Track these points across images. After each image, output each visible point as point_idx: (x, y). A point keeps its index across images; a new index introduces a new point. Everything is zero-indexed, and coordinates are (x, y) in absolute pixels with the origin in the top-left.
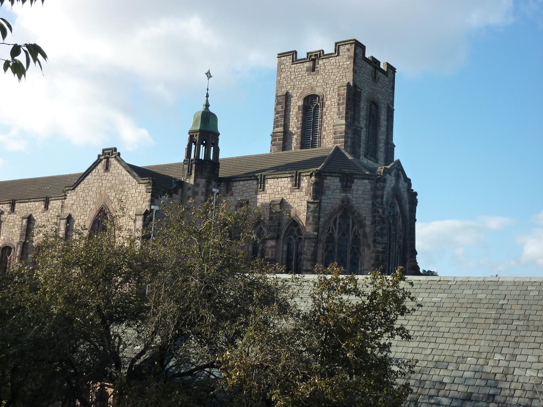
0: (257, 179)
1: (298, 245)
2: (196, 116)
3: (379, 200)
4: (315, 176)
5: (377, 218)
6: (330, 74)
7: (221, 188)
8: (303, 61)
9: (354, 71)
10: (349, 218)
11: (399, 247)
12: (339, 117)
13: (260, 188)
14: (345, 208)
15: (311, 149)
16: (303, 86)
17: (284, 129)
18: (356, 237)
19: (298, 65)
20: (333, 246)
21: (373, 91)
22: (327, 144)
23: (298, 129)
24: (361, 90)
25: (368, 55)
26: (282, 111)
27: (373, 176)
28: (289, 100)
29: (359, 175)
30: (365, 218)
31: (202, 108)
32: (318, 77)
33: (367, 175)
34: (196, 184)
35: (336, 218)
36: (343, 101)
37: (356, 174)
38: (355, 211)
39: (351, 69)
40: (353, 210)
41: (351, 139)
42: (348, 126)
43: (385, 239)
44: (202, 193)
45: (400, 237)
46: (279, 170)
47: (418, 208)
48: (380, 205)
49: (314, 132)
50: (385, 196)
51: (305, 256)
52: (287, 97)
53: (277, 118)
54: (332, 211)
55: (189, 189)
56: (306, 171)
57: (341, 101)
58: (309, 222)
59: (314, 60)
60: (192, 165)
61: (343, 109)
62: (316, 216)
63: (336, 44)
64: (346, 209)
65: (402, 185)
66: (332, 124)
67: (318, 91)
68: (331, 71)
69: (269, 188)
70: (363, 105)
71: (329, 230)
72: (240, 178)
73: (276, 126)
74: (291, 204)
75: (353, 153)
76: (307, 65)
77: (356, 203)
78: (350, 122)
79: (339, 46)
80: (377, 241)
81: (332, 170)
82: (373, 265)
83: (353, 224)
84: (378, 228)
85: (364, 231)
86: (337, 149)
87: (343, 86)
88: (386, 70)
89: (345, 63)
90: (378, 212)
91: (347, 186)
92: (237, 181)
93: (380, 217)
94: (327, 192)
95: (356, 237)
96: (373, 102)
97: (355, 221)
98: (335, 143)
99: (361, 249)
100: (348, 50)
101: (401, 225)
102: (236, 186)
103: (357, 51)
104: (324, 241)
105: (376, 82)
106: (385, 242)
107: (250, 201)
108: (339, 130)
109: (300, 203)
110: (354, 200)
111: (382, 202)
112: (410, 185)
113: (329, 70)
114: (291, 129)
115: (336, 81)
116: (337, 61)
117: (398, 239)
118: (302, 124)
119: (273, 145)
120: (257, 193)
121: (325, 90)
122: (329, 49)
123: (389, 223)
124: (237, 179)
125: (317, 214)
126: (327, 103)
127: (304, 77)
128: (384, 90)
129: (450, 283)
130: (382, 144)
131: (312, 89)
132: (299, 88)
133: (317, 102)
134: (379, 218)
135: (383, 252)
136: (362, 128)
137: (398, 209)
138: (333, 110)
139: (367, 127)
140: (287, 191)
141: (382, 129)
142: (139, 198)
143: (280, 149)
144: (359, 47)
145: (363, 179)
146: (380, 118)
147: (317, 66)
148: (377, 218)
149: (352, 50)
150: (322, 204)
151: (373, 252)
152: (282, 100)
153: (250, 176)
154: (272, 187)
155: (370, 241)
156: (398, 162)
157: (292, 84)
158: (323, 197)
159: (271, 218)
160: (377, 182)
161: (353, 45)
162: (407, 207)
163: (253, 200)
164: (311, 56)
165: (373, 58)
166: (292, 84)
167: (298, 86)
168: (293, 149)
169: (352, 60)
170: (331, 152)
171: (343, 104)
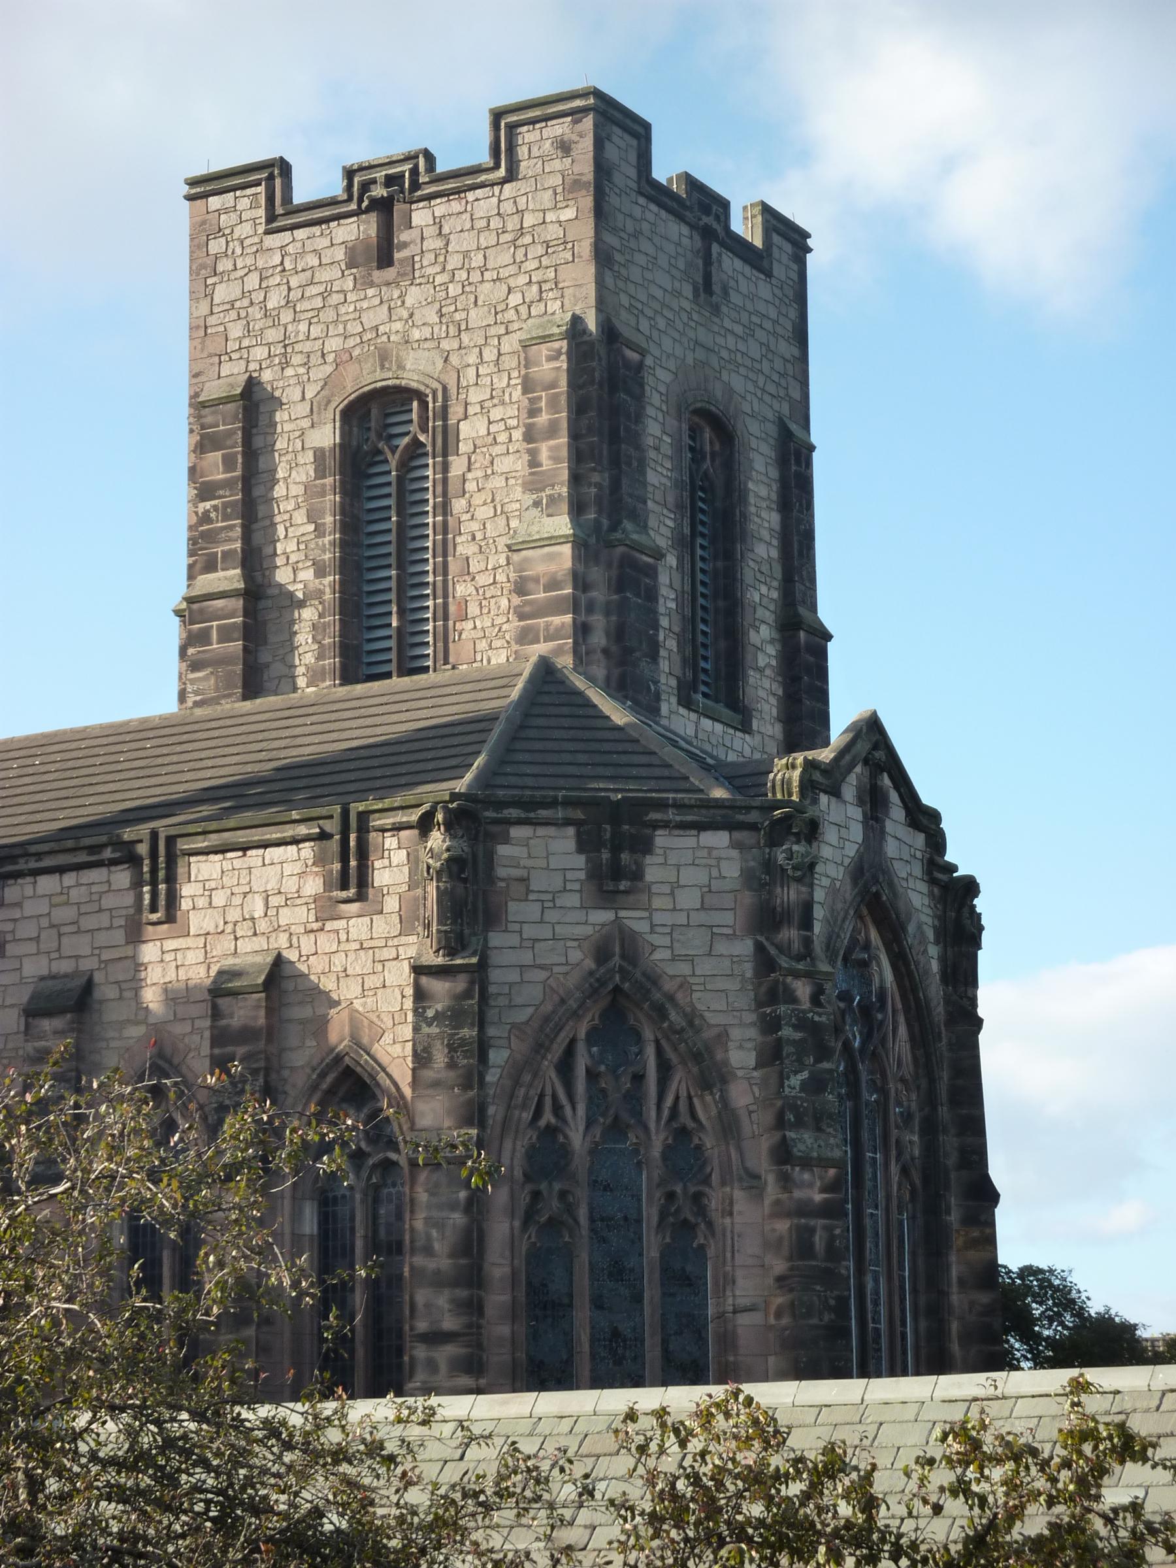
0: (133, 860)
1: (376, 1201)
3: (790, 934)
4: (449, 826)
5: (786, 1032)
6: (476, 277)
8: (323, 213)
9: (603, 257)
10: (638, 1038)
11: (905, 1171)
12: (537, 504)
13: (154, 909)
14: (617, 990)
15: (397, 682)
16: (333, 344)
17: (248, 576)
19: (300, 234)
20: (563, 1195)
21: (700, 354)
22: (482, 645)
23: (320, 573)
27: (749, 808)
28: (263, 420)
29: (679, 806)
30: (723, 1037)
32: (414, 295)
33: (718, 804)
35: (573, 1042)
36: (554, 414)
37: (662, 805)
38: (671, 998)
39: (585, 248)
40: (657, 996)
41: (607, 614)
42: (587, 546)
43: (834, 1145)
45: (907, 1117)
46: (250, 803)
47: (985, 959)
48: (800, 958)
49: (410, 587)
50: (819, 913)
51: (419, 1260)
53: (205, 518)
54: (548, 1008)
56: (397, 801)
57: (543, 419)
58: (428, 1074)
59: (384, 207)
61: (555, 459)
63: (497, 116)
64: (621, 993)
66: (502, 542)
67: (416, 368)
68: (477, 260)
70: (659, 431)
72: (39, 856)
73: (201, 558)
74: (327, 984)
75: (625, 686)
76: (349, 231)
79: (512, 127)
80: (798, 1150)
81: (532, 791)
82: (780, 1279)
83: (665, 1069)
85: (725, 1102)
86: (546, 671)
87: (545, 339)
88: (758, 243)
90: (792, 999)
91: (617, 872)
93: (801, 1024)
94: (512, 906)
95: (683, 1133)
96: (698, 412)
97: (671, 1055)
98: (526, 637)
99: (714, 1203)
100: (564, 147)
102: (18, 905)
103: (611, 153)
104: (518, 1173)
105: (716, 310)
106: (837, 1154)
107: (98, 977)
109: (372, 973)
110: (656, 940)
111: (807, 942)
112: (936, 841)
113: (466, 254)
114: (282, 576)
116: (508, 207)
117: (895, 1133)
118: (344, 545)
119: (195, 666)
120: (135, 935)
121: (454, 360)
122: (464, 144)
123: (847, 1046)
124: (22, 865)
125: (469, 1033)
126: (470, 430)
128: (755, 351)
130: (765, 632)
131: (383, 357)
132: (315, 359)
133: (414, 428)
134: (796, 1027)
135: (830, 1211)
136: (659, 555)
137: (885, 972)
139: (684, 543)
140: (298, 916)
141: (761, 550)
143: (229, 685)
144: (617, 128)
145: (700, 827)
148: (786, 1032)
149: (585, 146)
150: (495, 975)
151: (779, 1211)
152: (228, 424)
153: (93, 845)
154: (219, 899)
155: (758, 1152)
156: (871, 730)
157: (273, 335)
158: (496, 939)
160: (774, 842)
161: (588, 122)
162: (931, 958)
164: (365, 187)
165: (691, 182)
166: (273, 335)
167: (307, 347)
168: (301, 682)
169: (588, 202)
170: (515, 693)
171: (552, 431)
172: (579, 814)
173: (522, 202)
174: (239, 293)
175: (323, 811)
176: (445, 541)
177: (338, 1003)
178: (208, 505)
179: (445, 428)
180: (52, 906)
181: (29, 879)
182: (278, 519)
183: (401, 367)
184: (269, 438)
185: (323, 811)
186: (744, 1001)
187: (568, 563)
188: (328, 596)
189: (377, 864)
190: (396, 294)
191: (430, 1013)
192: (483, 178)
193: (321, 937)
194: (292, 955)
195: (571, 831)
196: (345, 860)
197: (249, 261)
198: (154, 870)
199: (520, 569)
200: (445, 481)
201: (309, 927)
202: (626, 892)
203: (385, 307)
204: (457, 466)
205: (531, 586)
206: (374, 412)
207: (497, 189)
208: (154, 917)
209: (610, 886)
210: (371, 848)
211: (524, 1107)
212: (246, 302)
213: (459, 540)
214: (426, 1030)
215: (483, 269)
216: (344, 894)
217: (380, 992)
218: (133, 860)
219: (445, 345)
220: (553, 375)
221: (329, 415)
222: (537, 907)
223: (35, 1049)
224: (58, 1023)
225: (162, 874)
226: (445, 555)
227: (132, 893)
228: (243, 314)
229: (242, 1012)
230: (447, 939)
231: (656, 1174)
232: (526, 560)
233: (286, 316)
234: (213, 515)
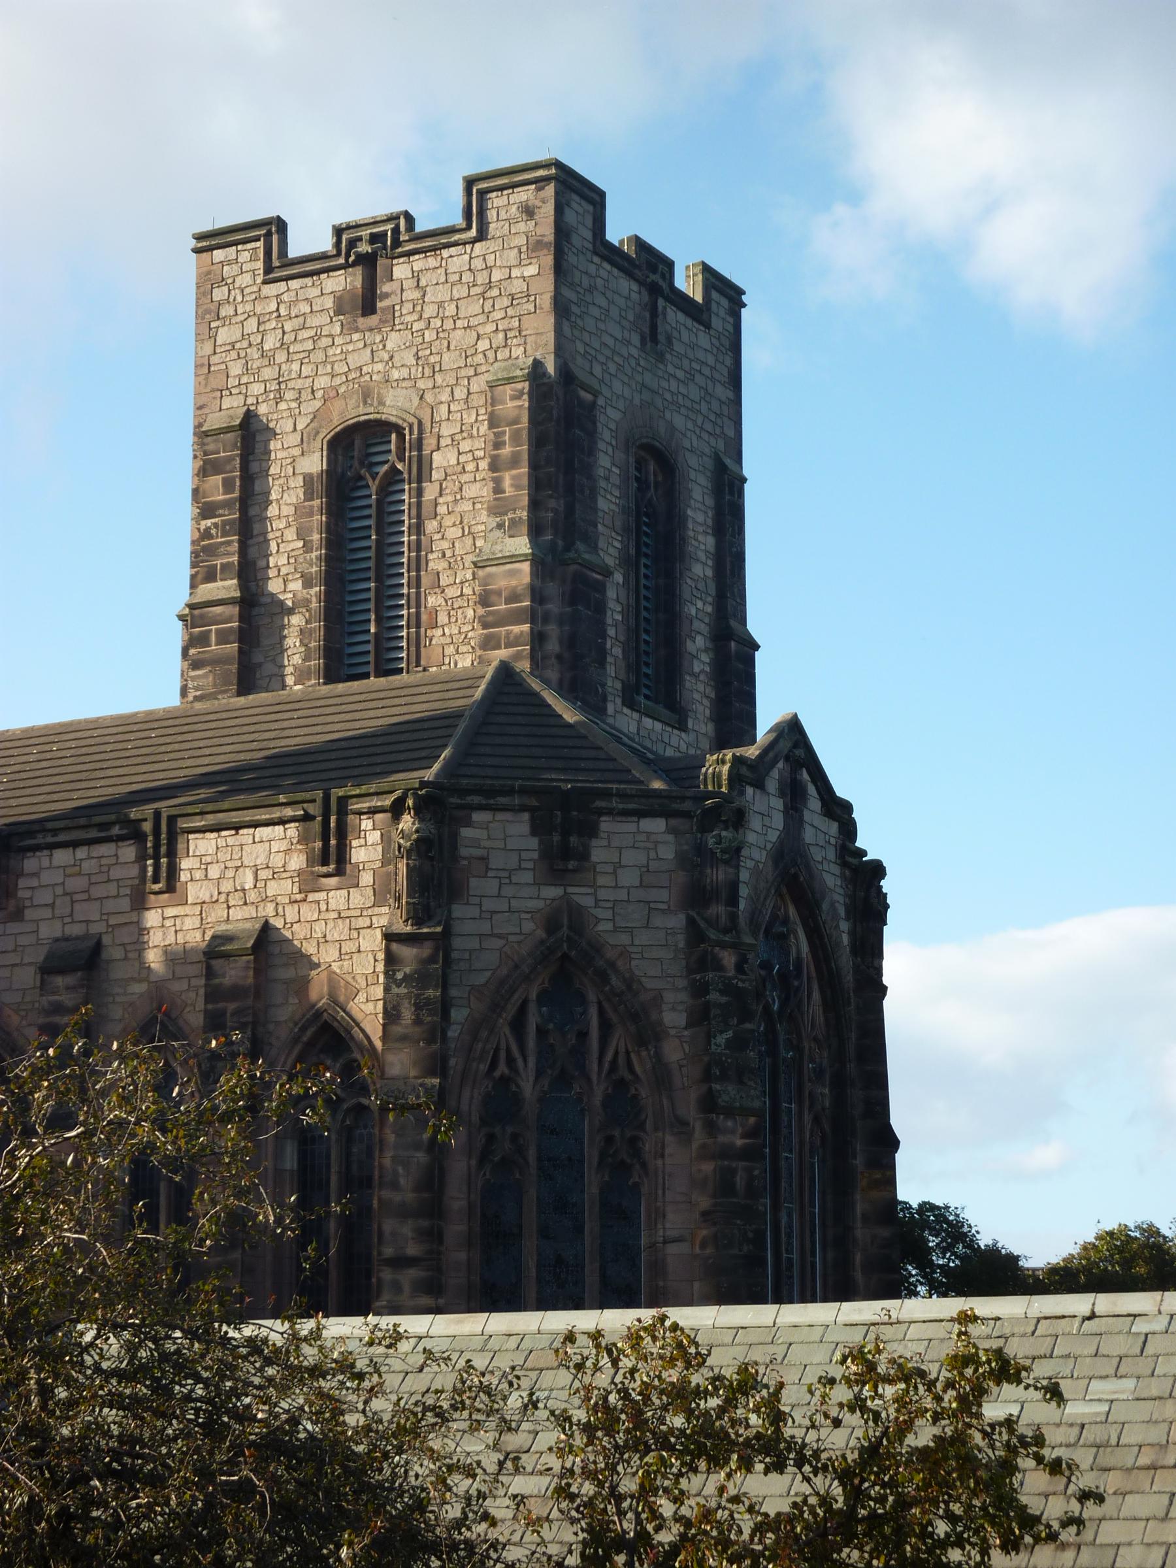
0: (138, 836)
3: (718, 910)
5: (714, 996)
6: (449, 324)
8: (314, 266)
9: (561, 309)
11: (816, 1120)
12: (500, 526)
13: (156, 880)
14: (565, 957)
16: (322, 382)
17: (244, 585)
18: (620, 1087)
19: (294, 284)
20: (515, 1137)
22: (450, 650)
23: (307, 584)
24: (596, 394)
25: (616, 233)
26: (226, 504)
28: (259, 448)
29: (622, 795)
30: (658, 999)
32: (394, 340)
33: (657, 794)
36: (516, 447)
37: (606, 794)
38: (612, 964)
39: (546, 300)
41: (561, 623)
42: (542, 563)
48: (726, 931)
49: (387, 597)
50: (744, 891)
51: (386, 1194)
52: (251, 435)
53: (206, 534)
54: (505, 971)
57: (507, 450)
58: (397, 1030)
59: (368, 262)
61: (517, 487)
62: (428, 1001)
63: (470, 182)
64: (568, 960)
65: (817, 829)
66: (469, 559)
67: (395, 405)
68: (450, 310)
69: (198, 875)
70: (608, 462)
71: (493, 1065)
72: (55, 832)
73: (203, 572)
74: (310, 948)
76: (338, 282)
77: (616, 930)
78: (553, 543)
79: (482, 193)
80: (723, 1100)
81: (487, 783)
82: (705, 1214)
83: (606, 1027)
84: (721, 1039)
85: (658, 1056)
86: (505, 672)
87: (509, 380)
88: (699, 298)
89: (516, 273)
90: (720, 967)
91: (566, 853)
93: (728, 988)
94: (473, 882)
98: (488, 643)
99: (648, 1146)
100: (529, 211)
101: (820, 1019)
102: (36, 875)
103: (570, 217)
104: (475, 1118)
105: (660, 357)
106: (757, 1104)
107: (106, 940)
108: (502, 583)
109: (347, 939)
111: (733, 917)
112: (849, 829)
113: (441, 305)
114: (274, 586)
115: (479, 358)
116: (478, 264)
119: (196, 665)
120: (139, 903)
121: (429, 397)
122: (439, 208)
123: (767, 1009)
124: (40, 839)
127: (325, 342)
128: (694, 393)
129: (1141, 1327)
130: (700, 641)
131: (366, 395)
132: (306, 395)
133: (392, 457)
134: (722, 992)
135: (747, 1154)
136: (608, 573)
138: (471, 491)
139: (629, 562)
140: (284, 888)
143: (227, 683)
144: (576, 196)
145: (641, 814)
146: (683, 520)
147: (386, 288)
148: (714, 996)
150: (457, 943)
152: (228, 452)
154: (214, 872)
155: (688, 1104)
156: (792, 732)
157: (268, 373)
158: (458, 911)
160: (704, 829)
161: (550, 190)
163: (125, 936)
164: (352, 243)
166: (268, 373)
167: (299, 384)
168: (290, 680)
169: (549, 260)
170: (479, 693)
173: (490, 259)
176: (418, 558)
177: (318, 965)
178: (209, 522)
179: (420, 457)
181: (46, 852)
182: (271, 536)
184: (264, 464)
187: (527, 579)
188: (314, 605)
189: (355, 843)
190: (378, 338)
191: (399, 976)
192: (456, 237)
193: (305, 908)
194: (278, 923)
195: (526, 816)
197: (249, 307)
198: (157, 846)
200: (419, 504)
201: (293, 898)
202: (574, 871)
203: (368, 350)
205: (494, 598)
207: (468, 247)
208: (156, 887)
210: (349, 829)
212: (245, 344)
213: (431, 556)
214: (395, 990)
216: (324, 869)
217: (355, 956)
218: (138, 836)
219: (421, 384)
220: (516, 412)
224: (70, 980)
225: (163, 849)
226: (418, 570)
227: (137, 866)
228: (242, 354)
229: (233, 972)
230: (415, 909)
232: (490, 575)
234: (213, 532)
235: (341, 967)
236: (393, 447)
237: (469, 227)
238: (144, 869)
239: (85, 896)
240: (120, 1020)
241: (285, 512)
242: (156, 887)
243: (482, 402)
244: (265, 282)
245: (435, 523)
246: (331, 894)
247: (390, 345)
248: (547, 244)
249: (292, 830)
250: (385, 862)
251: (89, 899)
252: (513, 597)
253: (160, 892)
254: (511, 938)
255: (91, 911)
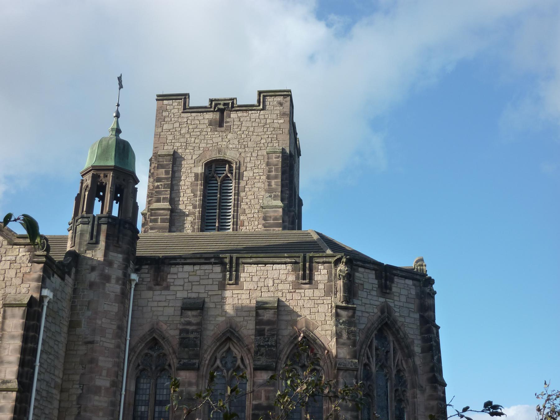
0: (223, 264)
2: (104, 143)
6: (251, 133)
7: (143, 276)
13: (230, 279)
16: (203, 145)
23: (195, 207)
28: (178, 163)
30: (413, 342)
31: (108, 134)
32: (230, 136)
34: (108, 262)
44: (118, 279)
52: (176, 159)
54: (369, 325)
55: (93, 269)
58: (341, 341)
59: (222, 111)
60: (99, 225)
63: (260, 93)
67: (230, 155)
74: (297, 309)
76: (210, 116)
77: (400, 316)
85: (414, 362)
87: (275, 152)
89: (275, 121)
92: (178, 264)
94: (360, 292)
110: (397, 310)
113: (248, 127)
115: (262, 145)
116: (262, 117)
120: (222, 287)
121: (243, 155)
127: (204, 133)
142: (12, 273)
145: (406, 278)
152: (167, 162)
154: (255, 279)
159: (259, 333)
166: (182, 140)
167: (194, 145)
172: (376, 267)
173: (266, 116)
174: (172, 127)
175: (297, 255)
176: (238, 203)
177: (301, 316)
178: (159, 184)
179: (239, 173)
180: (189, 275)
181: (181, 266)
182: (181, 191)
183: (225, 154)
184: (179, 168)
185: (297, 255)
186: (418, 332)
187: (281, 214)
188: (197, 214)
189: (316, 273)
190: (224, 135)
191: (341, 321)
192: (255, 108)
193: (294, 294)
194: (283, 299)
195: (374, 272)
196: (304, 270)
197: (176, 119)
198: (231, 267)
199: (265, 213)
200: (238, 187)
201: (290, 291)
202: (388, 293)
203: (221, 138)
204: (242, 184)
205: (268, 219)
206: (213, 166)
207: (259, 112)
208: (231, 282)
209: (384, 291)
210: (314, 268)
211: (364, 356)
212: (174, 130)
213: (242, 204)
214: (340, 326)
215: (253, 132)
216: (304, 281)
217: (316, 314)
218: (223, 264)
219: (240, 150)
220: (277, 162)
221: (200, 164)
222: (366, 294)
223: (185, 321)
224: (194, 313)
225: (234, 269)
226: (237, 207)
227: (221, 274)
228: (173, 133)
229: (268, 315)
230: (346, 298)
231: (394, 382)
232: (267, 211)
233: (187, 136)
234: (160, 187)
235: (311, 317)
236: (227, 169)
237: (259, 106)
238: (225, 276)
239: (198, 283)
240: (212, 330)
241: (187, 183)
242: (231, 282)
243: (262, 158)
244: (183, 112)
245: (244, 193)
246: (306, 290)
247: (229, 137)
248: (287, 115)
249: (289, 267)
250: (329, 280)
251: (200, 284)
252: (275, 219)
253: (232, 284)
254: (371, 314)
255: (201, 289)
